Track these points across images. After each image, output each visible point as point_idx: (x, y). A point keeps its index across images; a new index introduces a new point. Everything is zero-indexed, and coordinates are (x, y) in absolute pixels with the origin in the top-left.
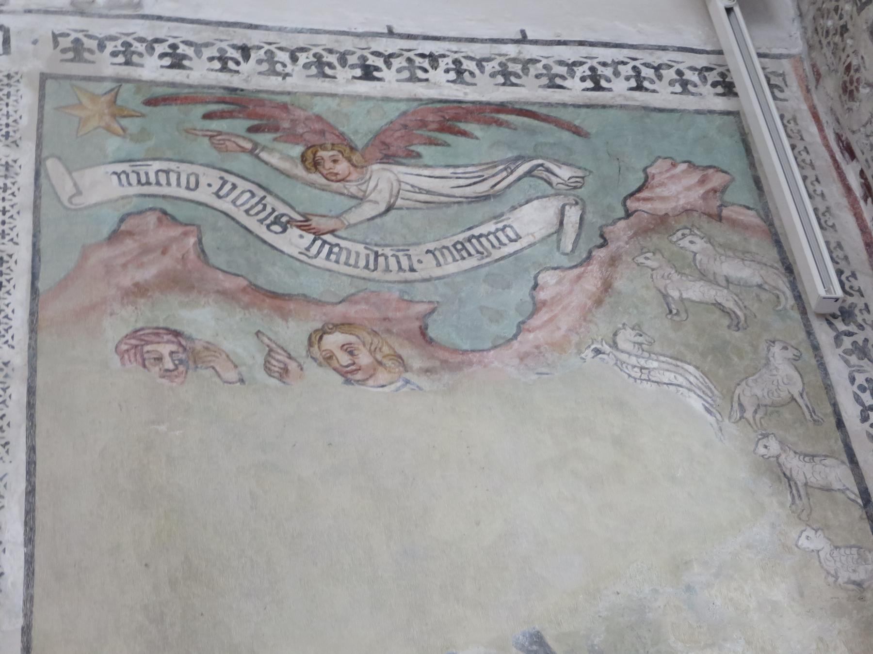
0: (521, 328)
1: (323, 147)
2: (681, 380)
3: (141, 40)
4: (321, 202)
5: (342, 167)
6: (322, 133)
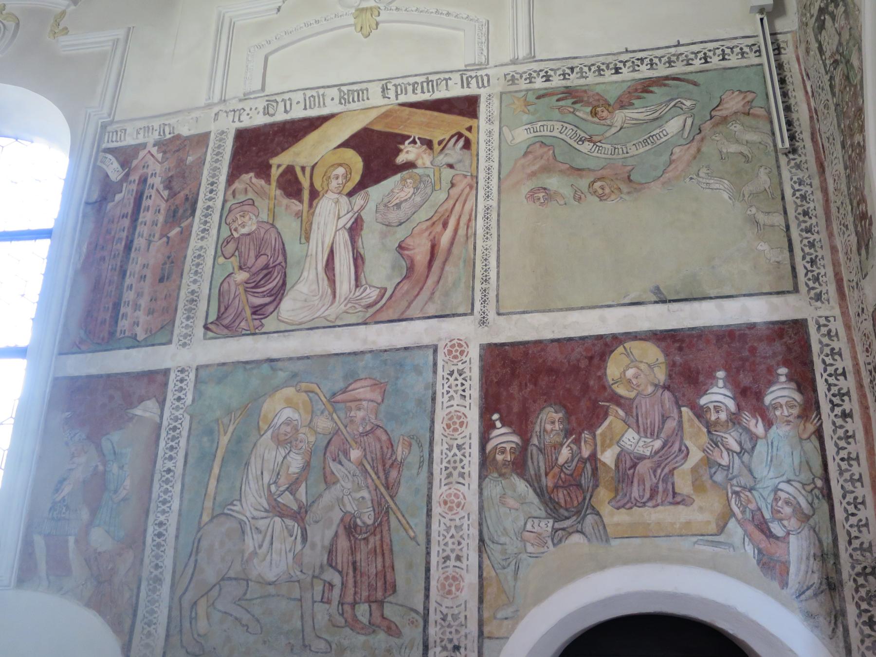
0: (663, 173)
1: (598, 106)
2: (721, 187)
3: (535, 71)
4: (594, 128)
5: (605, 114)
6: (598, 100)
